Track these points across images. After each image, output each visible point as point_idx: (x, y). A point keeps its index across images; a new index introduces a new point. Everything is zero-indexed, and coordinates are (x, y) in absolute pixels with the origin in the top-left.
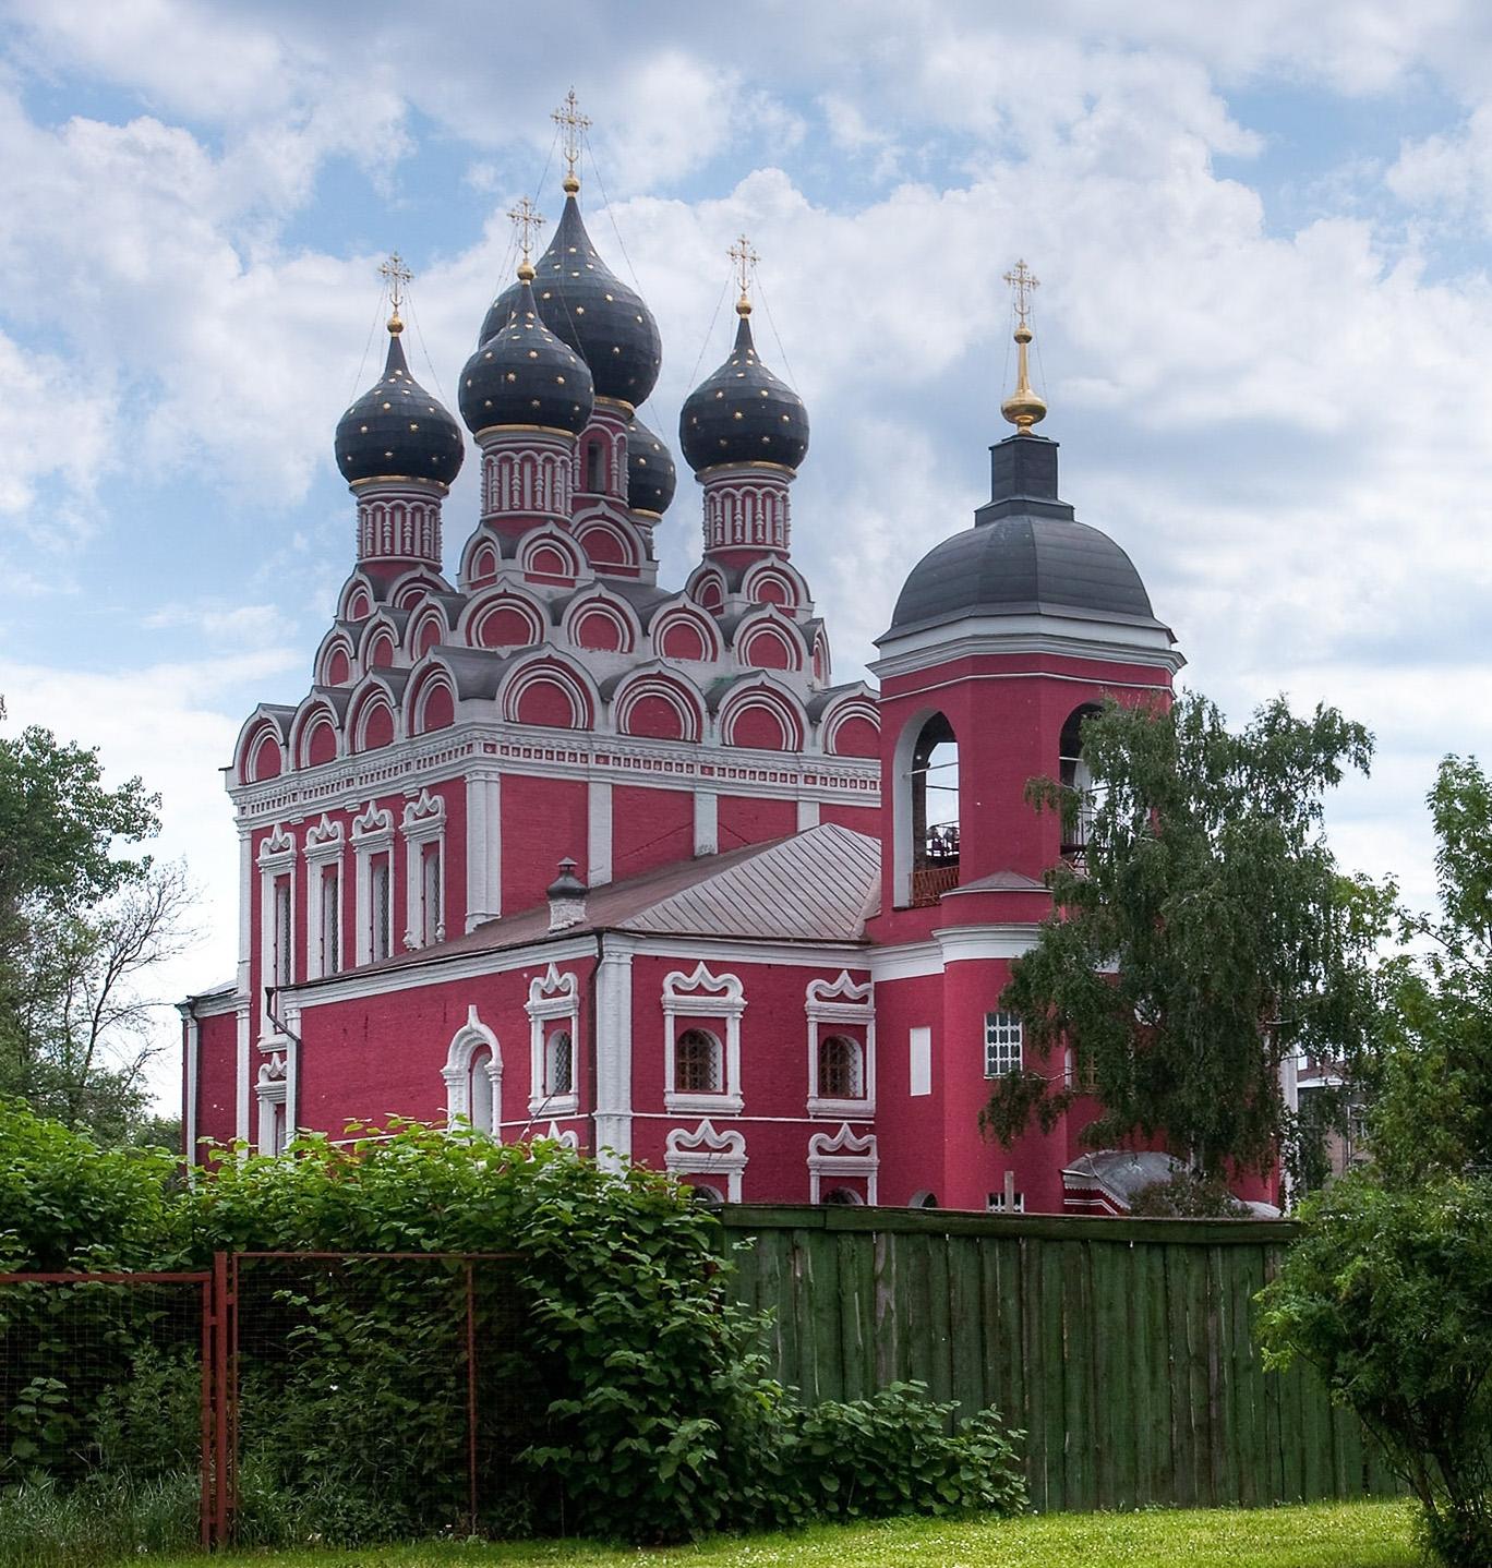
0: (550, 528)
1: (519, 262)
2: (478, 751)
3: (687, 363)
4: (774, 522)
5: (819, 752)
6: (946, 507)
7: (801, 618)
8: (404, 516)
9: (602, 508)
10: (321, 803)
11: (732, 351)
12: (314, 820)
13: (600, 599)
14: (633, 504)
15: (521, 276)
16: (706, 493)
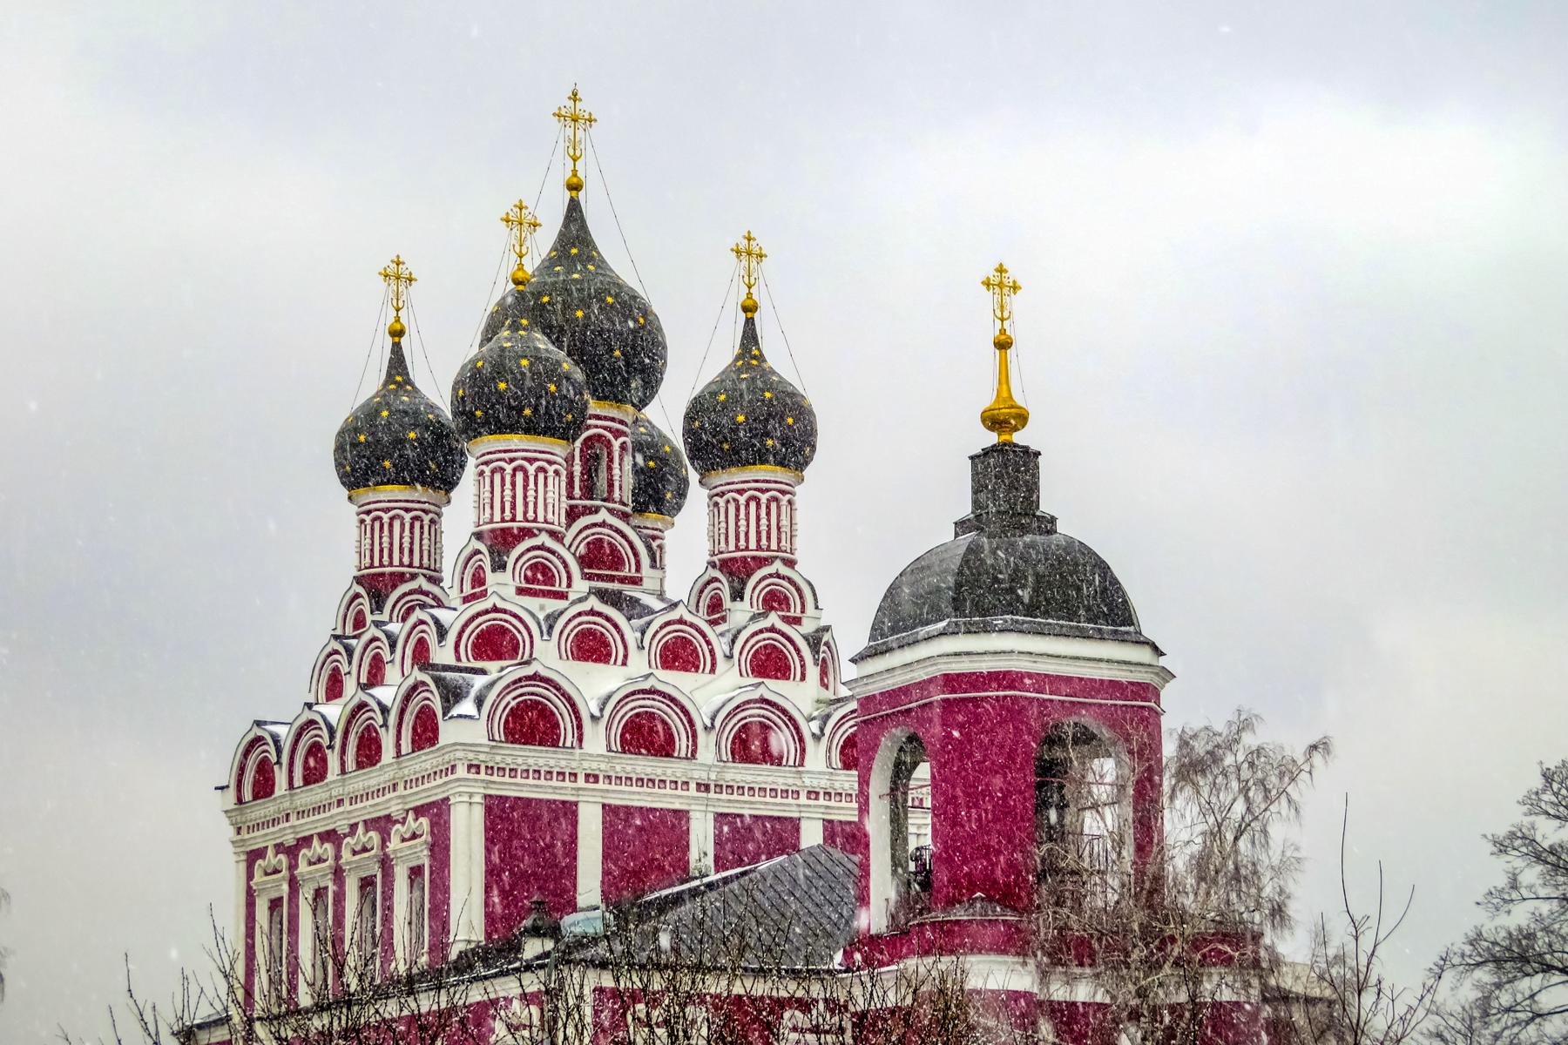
0: (544, 539)
1: (513, 267)
2: (461, 771)
3: (692, 366)
4: (779, 528)
5: (822, 766)
6: (932, 512)
7: (808, 627)
8: (402, 525)
9: (603, 515)
10: (313, 825)
11: (737, 350)
12: (306, 841)
13: (592, 612)
14: (640, 509)
15: (517, 282)
16: (711, 497)
